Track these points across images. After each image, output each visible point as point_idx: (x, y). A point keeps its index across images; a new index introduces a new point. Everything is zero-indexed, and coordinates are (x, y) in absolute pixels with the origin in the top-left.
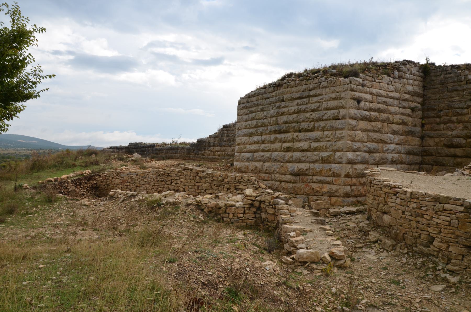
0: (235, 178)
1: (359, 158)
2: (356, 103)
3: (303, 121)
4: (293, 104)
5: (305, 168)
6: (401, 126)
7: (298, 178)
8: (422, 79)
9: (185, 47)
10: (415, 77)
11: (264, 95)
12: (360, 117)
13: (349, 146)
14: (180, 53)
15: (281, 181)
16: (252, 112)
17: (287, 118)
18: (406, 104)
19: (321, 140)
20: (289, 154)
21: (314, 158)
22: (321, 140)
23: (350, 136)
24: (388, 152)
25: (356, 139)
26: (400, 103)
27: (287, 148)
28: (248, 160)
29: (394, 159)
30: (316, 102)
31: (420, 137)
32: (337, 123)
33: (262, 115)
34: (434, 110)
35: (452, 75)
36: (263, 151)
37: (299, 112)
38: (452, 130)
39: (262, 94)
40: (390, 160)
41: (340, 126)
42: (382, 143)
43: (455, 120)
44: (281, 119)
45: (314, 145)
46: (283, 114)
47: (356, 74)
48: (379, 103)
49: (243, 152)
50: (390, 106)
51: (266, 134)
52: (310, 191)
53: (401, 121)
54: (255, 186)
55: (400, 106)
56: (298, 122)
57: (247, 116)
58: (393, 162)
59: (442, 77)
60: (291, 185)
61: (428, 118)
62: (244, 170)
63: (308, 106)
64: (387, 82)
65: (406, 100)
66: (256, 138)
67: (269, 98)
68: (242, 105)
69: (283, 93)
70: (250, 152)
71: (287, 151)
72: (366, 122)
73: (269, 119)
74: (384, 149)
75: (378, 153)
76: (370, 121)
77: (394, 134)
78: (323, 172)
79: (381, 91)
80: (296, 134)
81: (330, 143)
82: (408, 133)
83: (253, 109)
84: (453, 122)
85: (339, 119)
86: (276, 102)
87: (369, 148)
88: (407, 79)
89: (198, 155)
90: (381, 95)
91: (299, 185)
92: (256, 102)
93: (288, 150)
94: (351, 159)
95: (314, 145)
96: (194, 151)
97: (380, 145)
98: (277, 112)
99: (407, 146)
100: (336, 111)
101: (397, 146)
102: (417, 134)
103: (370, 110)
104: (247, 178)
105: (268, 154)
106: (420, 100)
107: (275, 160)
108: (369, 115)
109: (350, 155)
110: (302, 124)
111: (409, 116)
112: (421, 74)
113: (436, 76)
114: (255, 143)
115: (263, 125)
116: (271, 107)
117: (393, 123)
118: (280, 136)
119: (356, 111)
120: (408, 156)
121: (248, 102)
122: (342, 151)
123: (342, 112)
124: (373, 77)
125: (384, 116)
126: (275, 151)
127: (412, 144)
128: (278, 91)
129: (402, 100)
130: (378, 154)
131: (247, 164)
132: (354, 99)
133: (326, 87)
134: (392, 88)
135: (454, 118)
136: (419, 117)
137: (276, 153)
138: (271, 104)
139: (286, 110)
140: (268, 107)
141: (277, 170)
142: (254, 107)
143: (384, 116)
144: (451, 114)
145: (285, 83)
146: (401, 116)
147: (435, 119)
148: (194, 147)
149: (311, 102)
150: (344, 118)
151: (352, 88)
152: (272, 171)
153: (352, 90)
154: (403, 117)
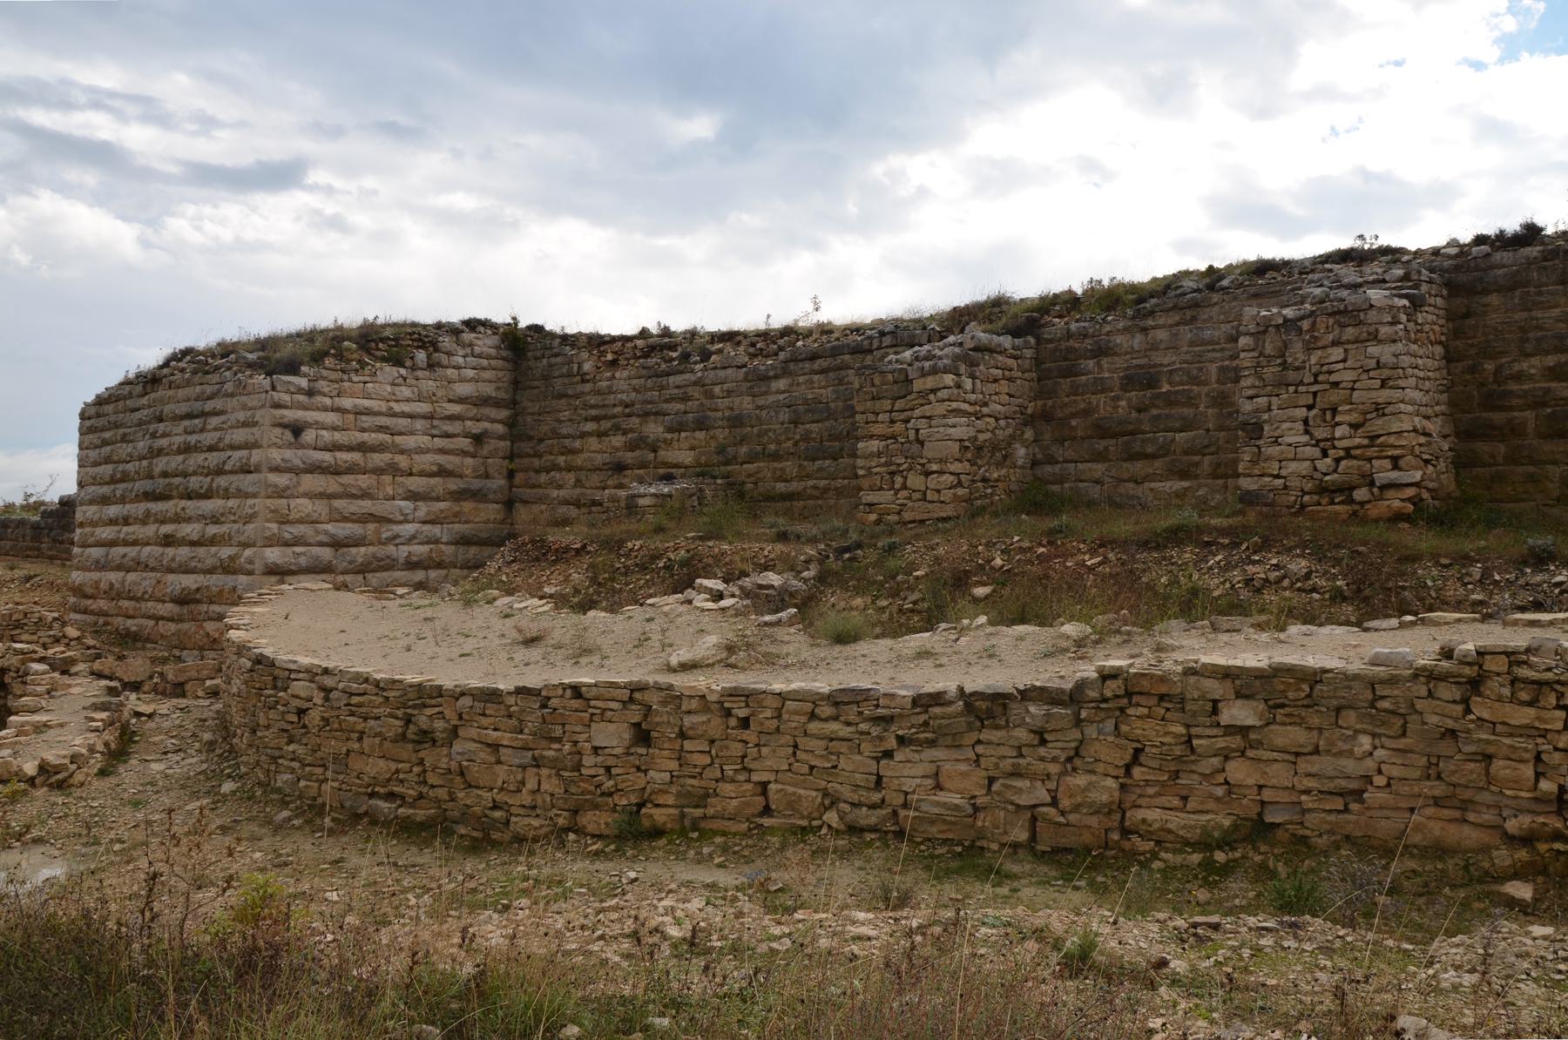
0: (11, 615)
1: (303, 561)
2: (288, 435)
3: (195, 473)
4: (180, 429)
5: (194, 587)
6: (437, 479)
7: (185, 609)
8: (508, 365)
9: (152, 112)
10: (485, 362)
11: (128, 402)
12: (302, 466)
13: (268, 534)
14: (137, 137)
15: (157, 618)
16: (105, 443)
17: (168, 463)
18: (449, 427)
19: (223, 519)
20: (170, 551)
21: (210, 562)
22: (223, 519)
23: (272, 511)
24: (397, 541)
25: (291, 518)
26: (433, 427)
27: (166, 536)
28: (100, 566)
29: (415, 559)
30: (215, 429)
31: (504, 503)
32: (246, 482)
33: (124, 450)
34: (531, 438)
35: (559, 360)
36: (126, 543)
37: (186, 449)
38: (560, 487)
39: (125, 398)
40: (401, 561)
41: (250, 490)
42: (378, 522)
43: (563, 464)
44: (157, 465)
45: (212, 530)
46: (160, 452)
47: (292, 368)
48: (363, 430)
49: (90, 546)
50: (401, 434)
51: (132, 501)
52: (205, 640)
53: (435, 468)
54: (51, 633)
55: (435, 432)
56: (185, 475)
57: (97, 451)
58: (318, 569)
59: (545, 361)
60: (173, 627)
61: (521, 456)
62: (89, 591)
63: (201, 437)
64: (390, 379)
65: (451, 418)
66: (113, 511)
67: (138, 410)
68: (88, 423)
69: (162, 401)
70: (102, 546)
71: (168, 545)
72: (322, 477)
73: (137, 463)
74: (384, 536)
75: (364, 545)
76: (338, 473)
77: (416, 500)
78: (226, 595)
79: (366, 403)
80: (183, 503)
81: (236, 526)
82: (459, 496)
83: (107, 435)
84: (555, 467)
85: (251, 472)
86: (150, 422)
87: (332, 536)
88: (459, 368)
89: (62, 542)
90: (369, 412)
91: (185, 626)
92: (112, 418)
93: (168, 541)
94: (276, 565)
95: (212, 530)
96: (51, 530)
97: (371, 527)
98: (150, 448)
99: (457, 527)
100: (244, 453)
101: (427, 527)
102: (491, 497)
103: (336, 447)
104: (37, 615)
105: (132, 552)
106: (504, 413)
107: (147, 566)
108: (332, 459)
109: (273, 555)
110: (193, 479)
111: (465, 453)
112: (504, 353)
113: (536, 358)
114: (113, 522)
115: (125, 478)
116: (141, 434)
117: (411, 474)
118: (157, 507)
119: (288, 454)
120: (462, 549)
121: (98, 415)
122: (253, 545)
123: (256, 456)
124: (343, 372)
125: (378, 459)
126: (148, 544)
127: (478, 519)
128: (153, 395)
129: (441, 419)
130: (363, 549)
131: (95, 575)
132: (285, 426)
133: (232, 395)
134: (406, 392)
135: (561, 460)
136: (501, 454)
137: (148, 549)
138: (140, 424)
139: (164, 442)
140: (135, 432)
141: (150, 590)
142: (110, 429)
143: (378, 459)
144: (556, 449)
145: (165, 376)
146: (436, 457)
147: (532, 460)
148: (50, 520)
149: (208, 427)
150: (257, 470)
151: (276, 400)
152: (139, 595)
153: (277, 406)
154: (442, 459)
